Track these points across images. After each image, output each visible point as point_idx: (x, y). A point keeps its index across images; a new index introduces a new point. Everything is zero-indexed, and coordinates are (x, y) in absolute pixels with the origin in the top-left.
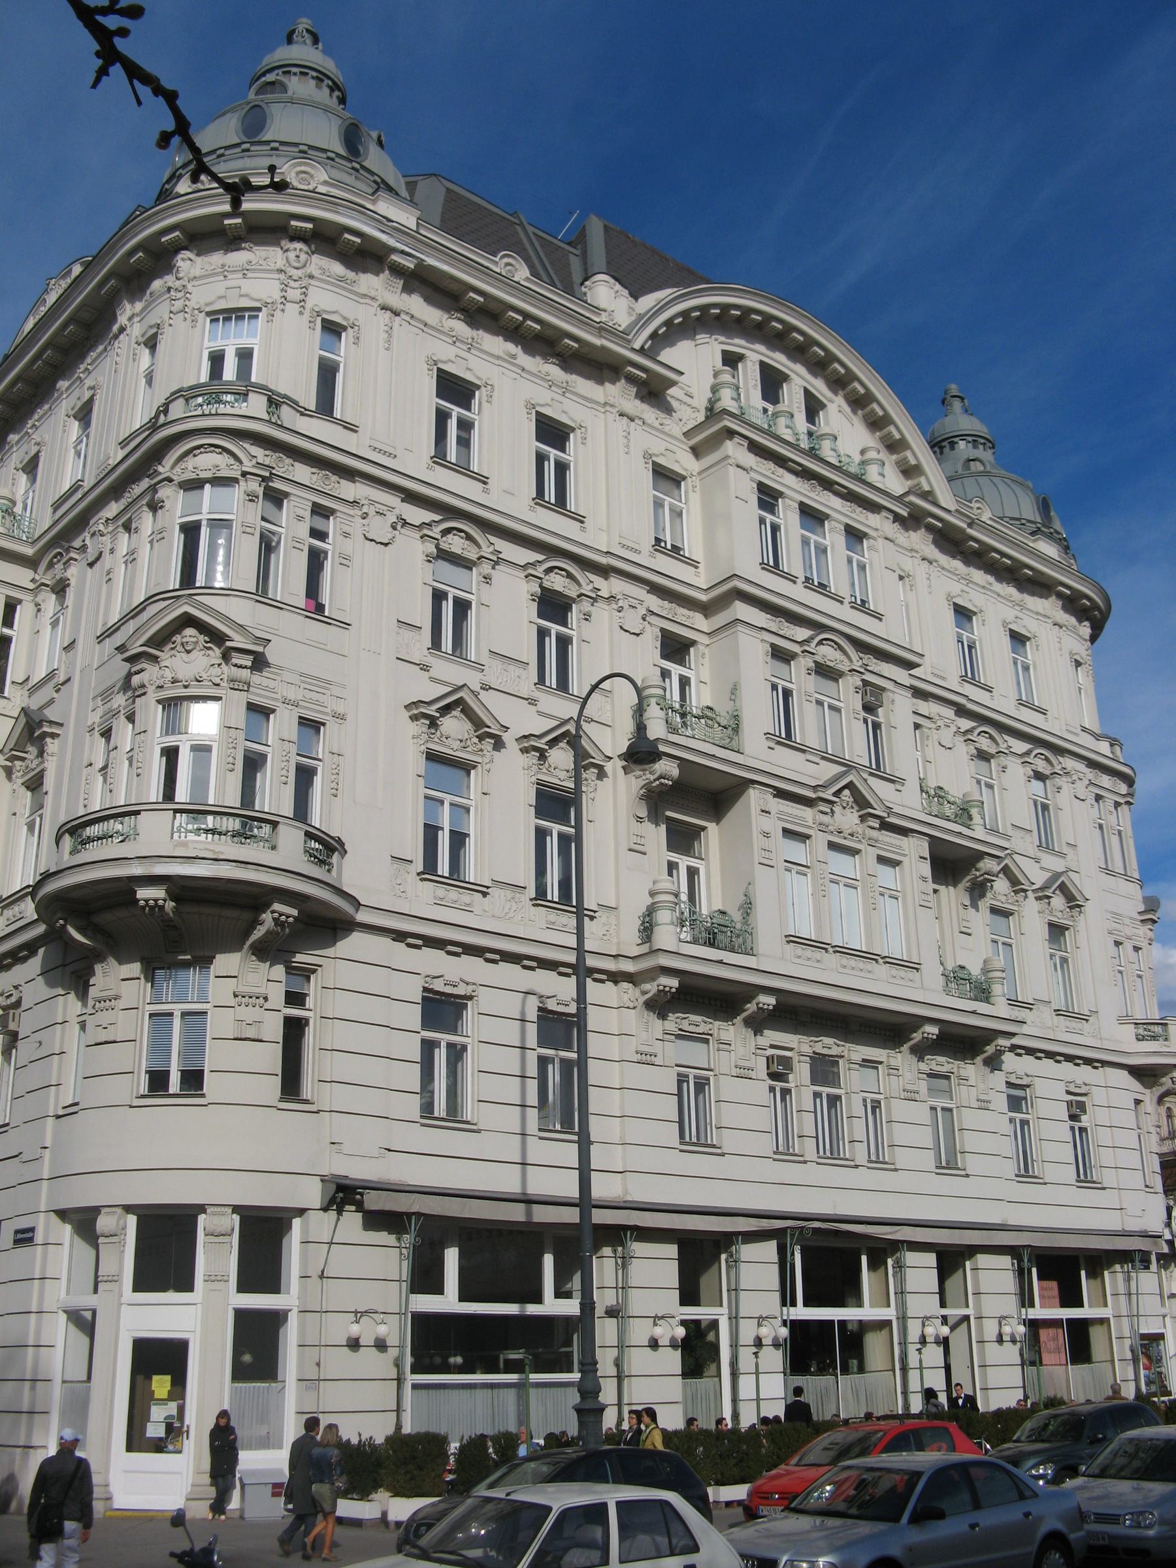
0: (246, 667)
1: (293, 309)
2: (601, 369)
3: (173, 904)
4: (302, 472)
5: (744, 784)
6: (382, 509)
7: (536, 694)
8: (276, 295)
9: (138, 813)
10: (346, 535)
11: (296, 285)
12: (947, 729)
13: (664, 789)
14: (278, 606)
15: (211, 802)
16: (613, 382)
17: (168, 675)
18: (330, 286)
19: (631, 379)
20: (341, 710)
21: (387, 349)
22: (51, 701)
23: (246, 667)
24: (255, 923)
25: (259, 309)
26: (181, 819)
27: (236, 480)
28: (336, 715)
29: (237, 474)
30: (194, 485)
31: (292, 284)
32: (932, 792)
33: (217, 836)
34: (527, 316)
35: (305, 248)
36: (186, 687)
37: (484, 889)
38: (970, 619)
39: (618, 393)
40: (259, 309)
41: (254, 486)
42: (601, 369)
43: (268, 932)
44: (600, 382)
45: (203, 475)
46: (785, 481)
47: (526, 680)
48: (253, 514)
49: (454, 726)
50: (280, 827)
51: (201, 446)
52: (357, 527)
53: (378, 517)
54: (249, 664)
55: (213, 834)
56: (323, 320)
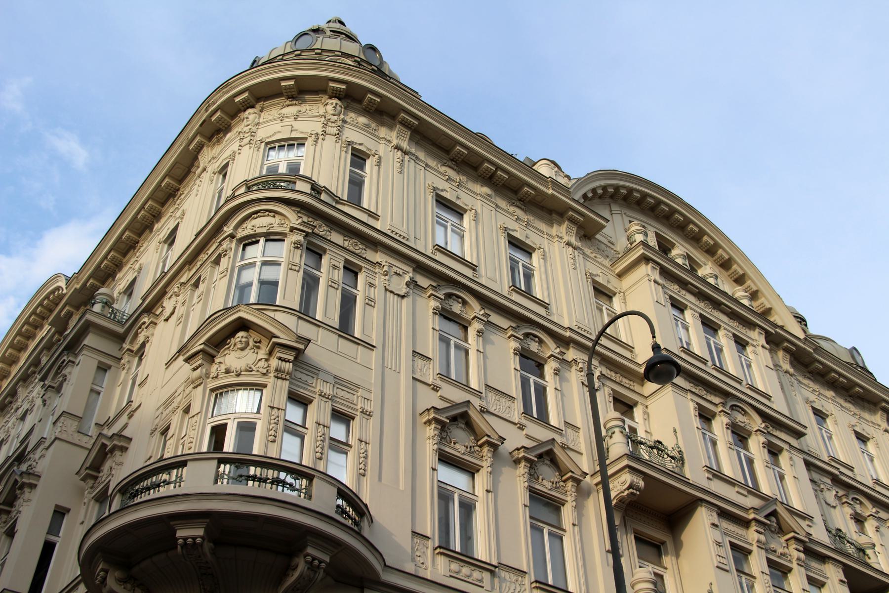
0: (288, 361)
1: (330, 140)
2: (551, 214)
3: (211, 544)
4: (337, 238)
5: (695, 503)
6: (399, 271)
7: (524, 421)
8: (319, 130)
9: (183, 464)
10: (371, 285)
11: (333, 125)
12: (828, 492)
13: (635, 499)
14: (318, 324)
15: (255, 452)
16: (560, 224)
17: (223, 368)
18: (357, 130)
19: (572, 221)
20: (368, 408)
21: (400, 172)
22: (125, 426)
23: (288, 361)
24: (289, 568)
25: (306, 139)
26: (226, 468)
27: (285, 235)
28: (363, 412)
29: (286, 230)
30: (250, 241)
31: (330, 124)
32: (834, 532)
33: (257, 483)
34: (498, 167)
35: (339, 103)
36: (238, 375)
37: (493, 568)
38: (824, 419)
39: (564, 231)
40: (306, 139)
41: (299, 237)
42: (551, 214)
43: (301, 576)
44: (551, 223)
45: (259, 231)
46: (688, 298)
47: (516, 412)
48: (299, 257)
49: (459, 434)
50: (315, 480)
51: (259, 211)
52: (380, 281)
53: (395, 277)
54: (292, 358)
55: (254, 481)
56: (353, 149)
